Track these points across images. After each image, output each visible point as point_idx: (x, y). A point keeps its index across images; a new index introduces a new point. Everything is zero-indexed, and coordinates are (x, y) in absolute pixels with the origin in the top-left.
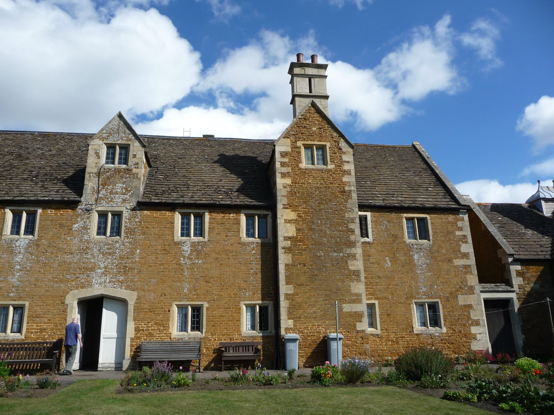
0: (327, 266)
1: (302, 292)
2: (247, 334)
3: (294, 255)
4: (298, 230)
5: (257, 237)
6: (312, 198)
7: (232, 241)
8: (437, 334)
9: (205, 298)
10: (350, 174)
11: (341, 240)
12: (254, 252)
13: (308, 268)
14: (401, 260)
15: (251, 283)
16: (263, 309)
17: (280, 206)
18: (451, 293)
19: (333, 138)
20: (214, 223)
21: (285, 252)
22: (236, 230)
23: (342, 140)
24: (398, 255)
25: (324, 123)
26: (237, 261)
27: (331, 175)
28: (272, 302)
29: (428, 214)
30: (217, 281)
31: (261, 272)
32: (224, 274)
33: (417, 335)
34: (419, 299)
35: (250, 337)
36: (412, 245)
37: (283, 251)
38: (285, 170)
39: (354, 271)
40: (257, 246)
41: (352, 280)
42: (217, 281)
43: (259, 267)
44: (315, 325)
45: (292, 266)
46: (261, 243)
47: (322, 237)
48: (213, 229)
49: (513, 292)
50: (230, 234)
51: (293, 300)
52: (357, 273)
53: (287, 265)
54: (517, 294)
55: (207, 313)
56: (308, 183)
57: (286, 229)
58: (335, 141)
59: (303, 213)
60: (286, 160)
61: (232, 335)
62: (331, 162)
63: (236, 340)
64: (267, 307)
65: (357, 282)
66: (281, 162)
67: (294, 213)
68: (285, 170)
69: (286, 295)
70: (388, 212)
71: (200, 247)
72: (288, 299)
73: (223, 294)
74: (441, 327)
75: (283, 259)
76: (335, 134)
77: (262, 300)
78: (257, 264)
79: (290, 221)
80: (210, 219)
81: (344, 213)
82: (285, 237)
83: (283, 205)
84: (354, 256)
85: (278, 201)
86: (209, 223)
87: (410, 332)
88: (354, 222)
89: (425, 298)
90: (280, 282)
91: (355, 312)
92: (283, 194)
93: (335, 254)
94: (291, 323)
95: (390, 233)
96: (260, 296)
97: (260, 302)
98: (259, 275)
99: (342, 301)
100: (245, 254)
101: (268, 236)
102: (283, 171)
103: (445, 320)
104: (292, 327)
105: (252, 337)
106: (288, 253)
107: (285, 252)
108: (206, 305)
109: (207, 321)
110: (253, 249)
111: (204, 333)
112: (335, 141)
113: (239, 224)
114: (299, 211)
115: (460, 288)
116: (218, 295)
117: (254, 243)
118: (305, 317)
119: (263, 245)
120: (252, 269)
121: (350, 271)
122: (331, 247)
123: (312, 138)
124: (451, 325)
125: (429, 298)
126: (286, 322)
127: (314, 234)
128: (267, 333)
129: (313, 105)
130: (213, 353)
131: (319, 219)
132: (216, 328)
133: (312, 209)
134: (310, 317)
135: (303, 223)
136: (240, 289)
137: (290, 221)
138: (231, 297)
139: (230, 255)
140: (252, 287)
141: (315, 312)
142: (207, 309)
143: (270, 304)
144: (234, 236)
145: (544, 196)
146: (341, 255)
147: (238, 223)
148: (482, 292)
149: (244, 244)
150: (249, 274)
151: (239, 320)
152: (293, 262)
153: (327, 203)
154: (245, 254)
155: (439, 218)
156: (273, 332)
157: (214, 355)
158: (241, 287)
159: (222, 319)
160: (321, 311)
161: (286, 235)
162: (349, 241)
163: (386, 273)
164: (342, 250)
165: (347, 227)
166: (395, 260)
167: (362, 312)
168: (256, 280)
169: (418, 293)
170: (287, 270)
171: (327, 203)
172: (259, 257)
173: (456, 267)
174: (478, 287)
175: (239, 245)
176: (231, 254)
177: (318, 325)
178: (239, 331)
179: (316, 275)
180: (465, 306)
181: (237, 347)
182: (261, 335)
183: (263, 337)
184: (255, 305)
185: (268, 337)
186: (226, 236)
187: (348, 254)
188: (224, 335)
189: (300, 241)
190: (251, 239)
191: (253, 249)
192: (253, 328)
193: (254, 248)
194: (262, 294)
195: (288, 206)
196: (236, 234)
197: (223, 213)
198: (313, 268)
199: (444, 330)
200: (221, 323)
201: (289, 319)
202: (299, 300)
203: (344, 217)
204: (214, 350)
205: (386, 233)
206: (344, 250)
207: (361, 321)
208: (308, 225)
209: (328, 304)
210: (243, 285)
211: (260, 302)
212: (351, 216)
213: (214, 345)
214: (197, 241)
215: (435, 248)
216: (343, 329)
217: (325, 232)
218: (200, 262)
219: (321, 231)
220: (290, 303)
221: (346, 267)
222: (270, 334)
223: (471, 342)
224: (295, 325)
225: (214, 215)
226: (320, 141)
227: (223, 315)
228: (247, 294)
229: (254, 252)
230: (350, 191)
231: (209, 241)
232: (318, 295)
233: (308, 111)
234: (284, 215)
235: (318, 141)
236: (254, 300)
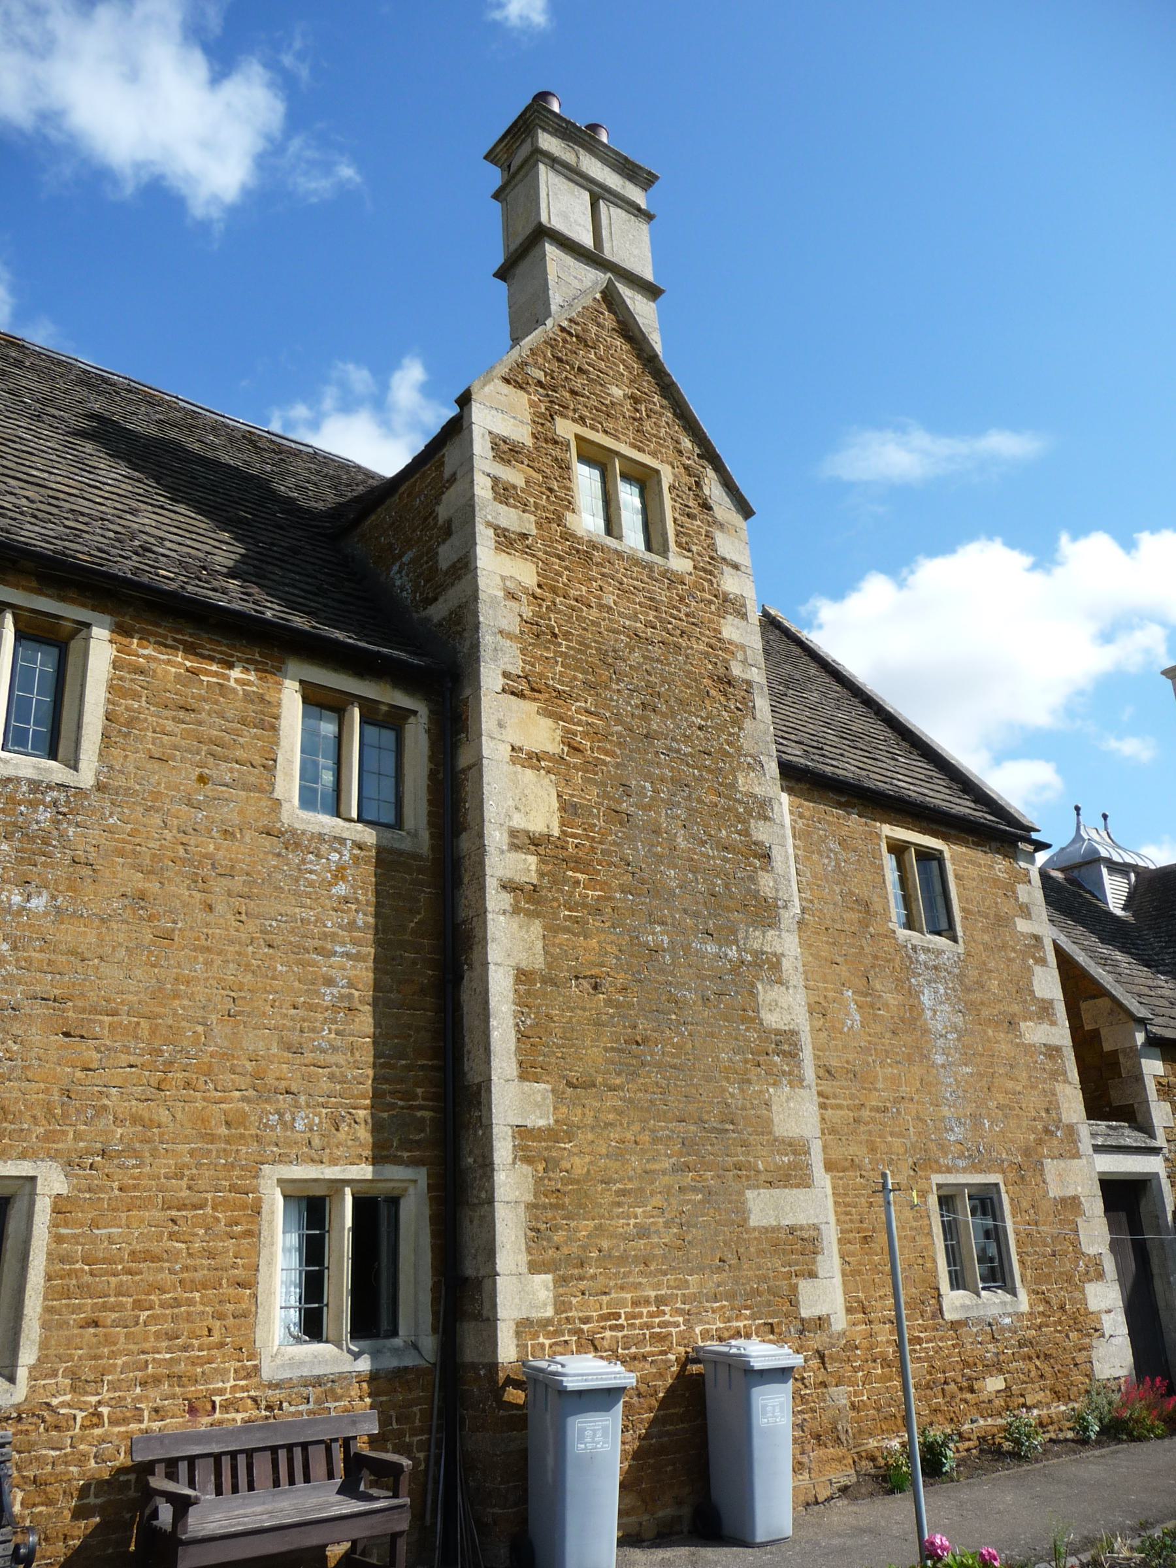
0: (685, 1003)
1: (590, 1121)
2: (292, 1363)
3: (552, 929)
4: (568, 809)
5: (354, 815)
6: (620, 676)
7: (229, 814)
8: (1007, 1320)
9: (48, 1137)
10: (744, 617)
11: (727, 886)
12: (341, 889)
13: (609, 1002)
14: (886, 1006)
15: (322, 1058)
16: (373, 1212)
17: (491, 678)
18: (1027, 1152)
19: (680, 452)
20: (136, 696)
21: (516, 910)
22: (257, 760)
23: (710, 473)
24: (878, 987)
25: (647, 383)
26: (252, 926)
27: (682, 599)
28: (421, 1175)
29: (945, 838)
30: (133, 1032)
31: (375, 1003)
32: (176, 995)
33: (955, 1325)
34: (949, 1170)
35: (307, 1382)
36: (914, 948)
37: (506, 899)
38: (511, 518)
39: (778, 1032)
40: (356, 859)
41: (775, 1077)
42: (133, 1032)
43: (365, 973)
44: (647, 1302)
45: (544, 982)
46: (380, 850)
47: (660, 858)
48: (130, 723)
49: (1155, 1151)
50: (224, 772)
51: (551, 1164)
52: (785, 1044)
53: (523, 976)
54: (1167, 1160)
55: (59, 1239)
56: (601, 607)
57: (516, 801)
58: (686, 468)
59: (585, 734)
60: (514, 476)
61: (206, 1378)
62: (679, 545)
63: (225, 1408)
64: (394, 1201)
65: (790, 1083)
66: (496, 480)
67: (549, 722)
68: (511, 518)
69: (522, 1132)
70: (840, 805)
71: (44, 816)
72: (528, 1160)
73: (164, 1116)
74: (1013, 1292)
75: (508, 944)
76: (687, 443)
77: (377, 1160)
78: (357, 958)
79: (533, 760)
80: (116, 665)
81: (734, 771)
82: (513, 833)
83: (506, 675)
84: (770, 965)
85: (486, 654)
86: (111, 688)
87: (934, 1317)
88: (766, 818)
89: (965, 1170)
90: (495, 1063)
91: (792, 1230)
92: (504, 624)
93: (711, 948)
94: (542, 1286)
95: (851, 893)
96: (364, 1134)
97: (365, 1171)
98: (365, 1022)
99: (745, 1173)
100: (296, 894)
101: (409, 822)
102: (504, 523)
103: (1022, 1262)
104: (549, 1312)
105: (318, 1381)
106: (531, 915)
107: (516, 910)
108: (52, 1182)
109: (50, 1293)
110: (339, 873)
111: (22, 1373)
112: (686, 468)
113: (274, 729)
114: (570, 720)
115: (1047, 1131)
116: (136, 1119)
117: (342, 841)
118: (605, 1257)
119: (387, 862)
120: (330, 982)
121: (766, 1033)
122: (696, 915)
123: (610, 425)
124: (1038, 1281)
125: (975, 1168)
126: (521, 1294)
127: (631, 839)
128: (395, 1351)
129: (610, 298)
130: (79, 1513)
131: (648, 777)
132: (109, 1340)
133: (619, 722)
134: (623, 1260)
135: (586, 780)
136: (262, 1091)
137: (533, 760)
138: (212, 1138)
139: (219, 886)
140: (325, 1085)
141: (643, 1232)
142: (61, 1207)
143: (412, 1184)
144: (246, 788)
145: (1107, 855)
146: (733, 953)
147: (268, 723)
148: (1097, 1149)
149: (292, 840)
150: (312, 1008)
151: (248, 1284)
152: (549, 966)
153: (673, 714)
154: (296, 894)
155: (970, 862)
156: (429, 1343)
157: (84, 1527)
158: (270, 1080)
159: (149, 1273)
160: (667, 1225)
161: (519, 822)
162: (755, 895)
163: (851, 1057)
164: (734, 932)
165: (746, 833)
166: (872, 1006)
167: (816, 1228)
168: (345, 1045)
169: (943, 1148)
170: (523, 1001)
171: (673, 714)
172: (365, 919)
173: (1029, 1049)
174: (1087, 1131)
175: (267, 842)
176: (224, 881)
177: (660, 1301)
178: (246, 1350)
179: (646, 1040)
180: (1063, 1200)
181: (233, 1468)
182: (364, 1365)
183: (374, 1377)
184: (338, 1185)
185: (399, 1373)
186: (202, 779)
187: (757, 953)
188: (157, 1380)
189: (578, 863)
190: (325, 822)
191: (339, 873)
192: (312, 1326)
193: (341, 868)
194: (377, 1127)
195: (523, 686)
196: (254, 776)
197: (191, 650)
198: (631, 1006)
199: (1024, 1301)
200: (138, 1305)
201: (535, 1267)
202: (580, 1165)
203: (733, 786)
204: (84, 1491)
205: (837, 889)
206: (741, 935)
207: (812, 1275)
208: (605, 795)
209: (695, 1190)
210: (281, 1069)
211: (365, 1171)
212: (757, 790)
213: (83, 1459)
214: (30, 773)
215: (973, 974)
216: (753, 1317)
217: (672, 839)
218: (38, 903)
219: (656, 832)
220: (539, 1181)
221: (749, 1015)
222: (409, 1361)
223: (1091, 1347)
224: (561, 1306)
225: (144, 652)
226: (640, 450)
227: (155, 1247)
228: (300, 1125)
229: (341, 889)
230: (749, 683)
231: (100, 787)
232: (655, 1140)
233: (593, 315)
234: (510, 731)
235: (634, 446)
236: (334, 1162)
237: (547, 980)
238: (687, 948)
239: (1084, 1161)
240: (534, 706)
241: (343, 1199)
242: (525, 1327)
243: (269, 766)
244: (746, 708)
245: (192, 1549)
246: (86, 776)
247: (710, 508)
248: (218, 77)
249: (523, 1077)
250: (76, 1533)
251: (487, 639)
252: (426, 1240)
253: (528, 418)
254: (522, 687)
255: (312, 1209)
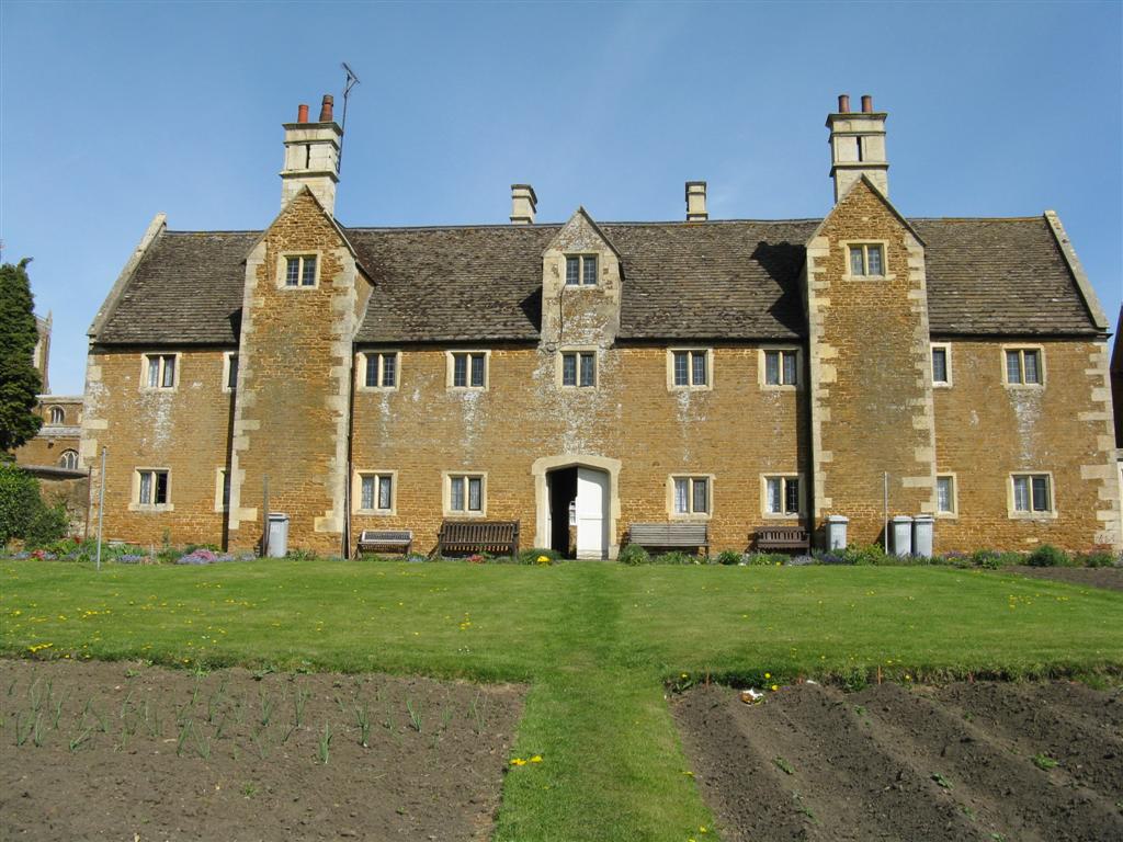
3: (833, 409)
4: (840, 373)
12: (777, 405)
16: (791, 483)
33: (1013, 521)
34: (1019, 470)
36: (1014, 391)
47: (874, 382)
53: (823, 423)
60: (822, 270)
68: (820, 285)
69: (823, 464)
75: (819, 415)
102: (818, 287)
108: (713, 477)
110: (777, 401)
126: (822, 502)
129: (864, 179)
142: (715, 482)
146: (903, 408)
149: (764, 394)
161: (823, 380)
170: (823, 430)
171: (883, 333)
189: (843, 389)
190: (774, 387)
191: (777, 401)
192: (777, 508)
195: (826, 339)
199: (1055, 514)
207: (928, 501)
218: (703, 419)
221: (909, 425)
229: (777, 405)
234: (820, 351)
237: (832, 424)
238: (883, 408)
239: (1109, 465)
240: (828, 345)
241: (439, 486)
242: (822, 510)
243: (756, 376)
244: (917, 321)
245: (919, 549)
246: (711, 389)
247: (906, 249)
248: (90, 353)
249: (823, 449)
250: (92, 528)
251: (812, 327)
252: (804, 490)
253: (828, 246)
254: (827, 339)
255: (775, 482)
